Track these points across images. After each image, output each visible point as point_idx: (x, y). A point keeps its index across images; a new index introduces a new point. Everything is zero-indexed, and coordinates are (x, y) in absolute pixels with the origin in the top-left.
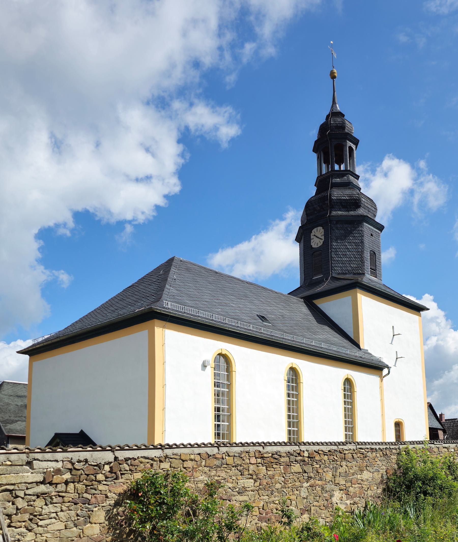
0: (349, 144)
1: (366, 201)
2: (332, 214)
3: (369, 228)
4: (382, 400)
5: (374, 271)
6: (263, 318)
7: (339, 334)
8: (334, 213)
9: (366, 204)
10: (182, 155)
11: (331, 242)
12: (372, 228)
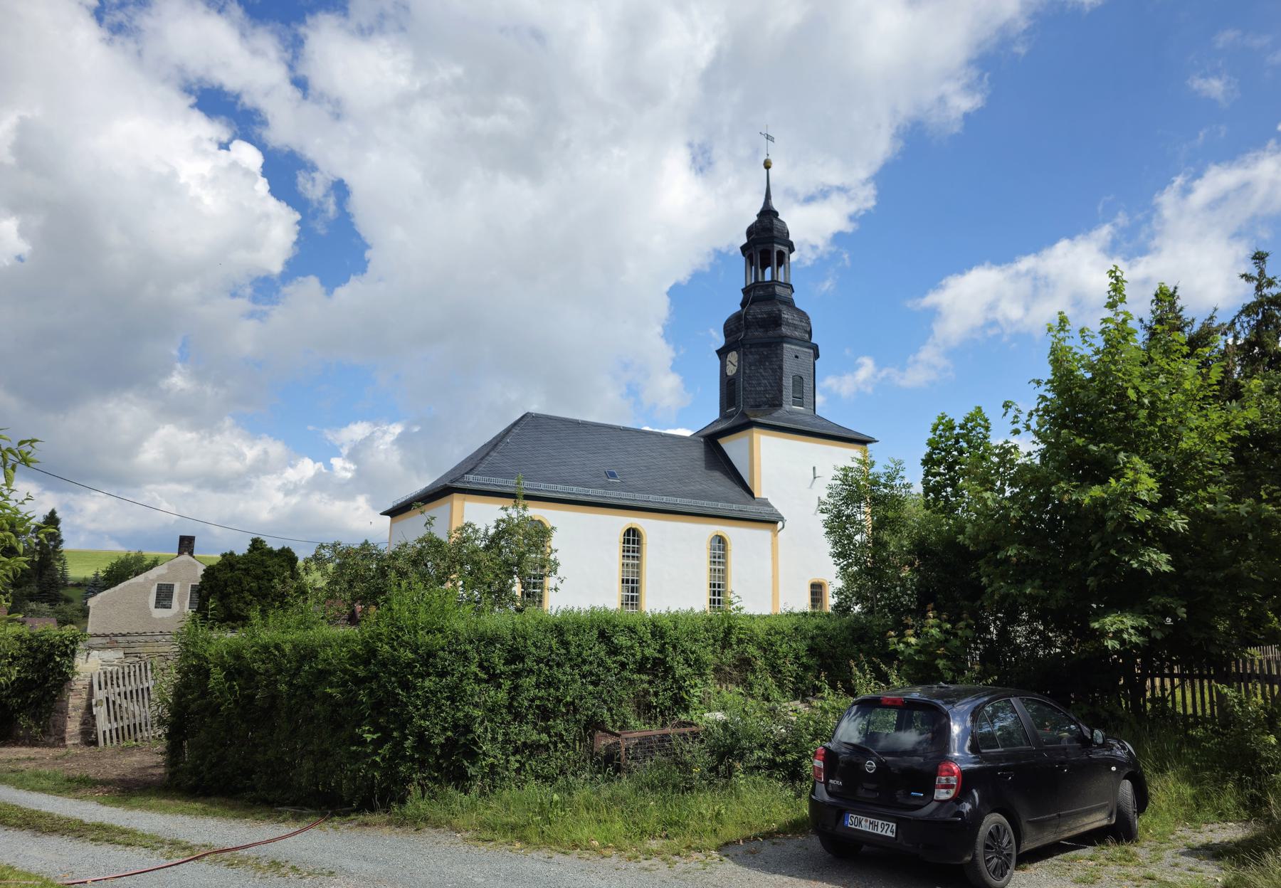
0: (778, 247)
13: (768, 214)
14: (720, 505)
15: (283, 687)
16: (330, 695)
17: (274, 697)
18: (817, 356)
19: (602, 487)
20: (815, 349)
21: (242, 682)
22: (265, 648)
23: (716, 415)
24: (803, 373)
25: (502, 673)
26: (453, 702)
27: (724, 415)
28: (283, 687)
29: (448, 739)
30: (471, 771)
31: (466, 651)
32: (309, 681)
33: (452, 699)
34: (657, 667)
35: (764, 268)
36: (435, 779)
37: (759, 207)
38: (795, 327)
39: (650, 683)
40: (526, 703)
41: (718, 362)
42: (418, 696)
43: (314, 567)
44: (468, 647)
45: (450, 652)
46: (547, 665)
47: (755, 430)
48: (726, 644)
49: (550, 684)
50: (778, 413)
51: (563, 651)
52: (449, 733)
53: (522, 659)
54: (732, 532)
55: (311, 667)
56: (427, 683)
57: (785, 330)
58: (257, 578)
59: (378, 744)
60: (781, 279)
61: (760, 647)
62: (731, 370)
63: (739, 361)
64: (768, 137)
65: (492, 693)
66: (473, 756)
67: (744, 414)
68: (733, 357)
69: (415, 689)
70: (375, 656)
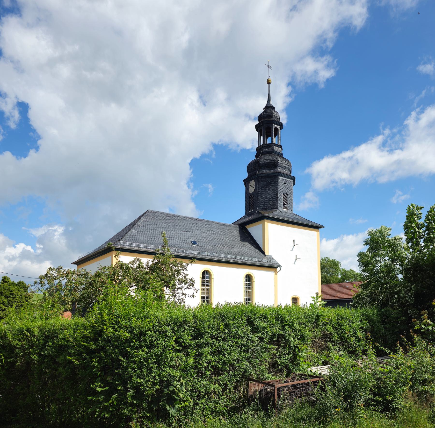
0: (275, 126)
1: (282, 162)
2: (260, 173)
3: (283, 179)
4: (276, 286)
5: (286, 205)
6: (194, 243)
7: (254, 247)
8: (261, 172)
9: (282, 165)
10: (290, 95)
11: (258, 190)
12: (285, 179)
13: (269, 108)
14: (250, 259)
15: (35, 357)
16: (71, 362)
17: (29, 363)
18: (294, 184)
19: (190, 249)
20: (294, 179)
21: (6, 353)
22: (21, 331)
23: (244, 214)
24: (288, 191)
25: (190, 345)
26: (159, 365)
27: (248, 213)
28: (35, 357)
29: (157, 390)
30: (172, 411)
31: (166, 331)
32: (53, 352)
33: (158, 363)
34: (278, 340)
35: (267, 137)
36: (148, 419)
37: (264, 103)
38: (284, 168)
39: (277, 350)
40: (205, 365)
41: (244, 188)
42: (135, 362)
43: (46, 282)
44: (167, 328)
45: (155, 332)
46: (217, 339)
47: (266, 220)
48: (316, 324)
49: (219, 352)
50: (276, 212)
51: (226, 331)
52: (157, 387)
53: (202, 337)
54: (255, 273)
55: (53, 343)
56: (140, 353)
57: (279, 169)
58: (7, 297)
59: (108, 395)
60: (275, 142)
61: (333, 327)
62: (251, 190)
63: (256, 185)
64: (269, 67)
65: (184, 359)
66: (172, 401)
67: (259, 213)
68: (252, 183)
69: (132, 357)
70: (100, 336)
